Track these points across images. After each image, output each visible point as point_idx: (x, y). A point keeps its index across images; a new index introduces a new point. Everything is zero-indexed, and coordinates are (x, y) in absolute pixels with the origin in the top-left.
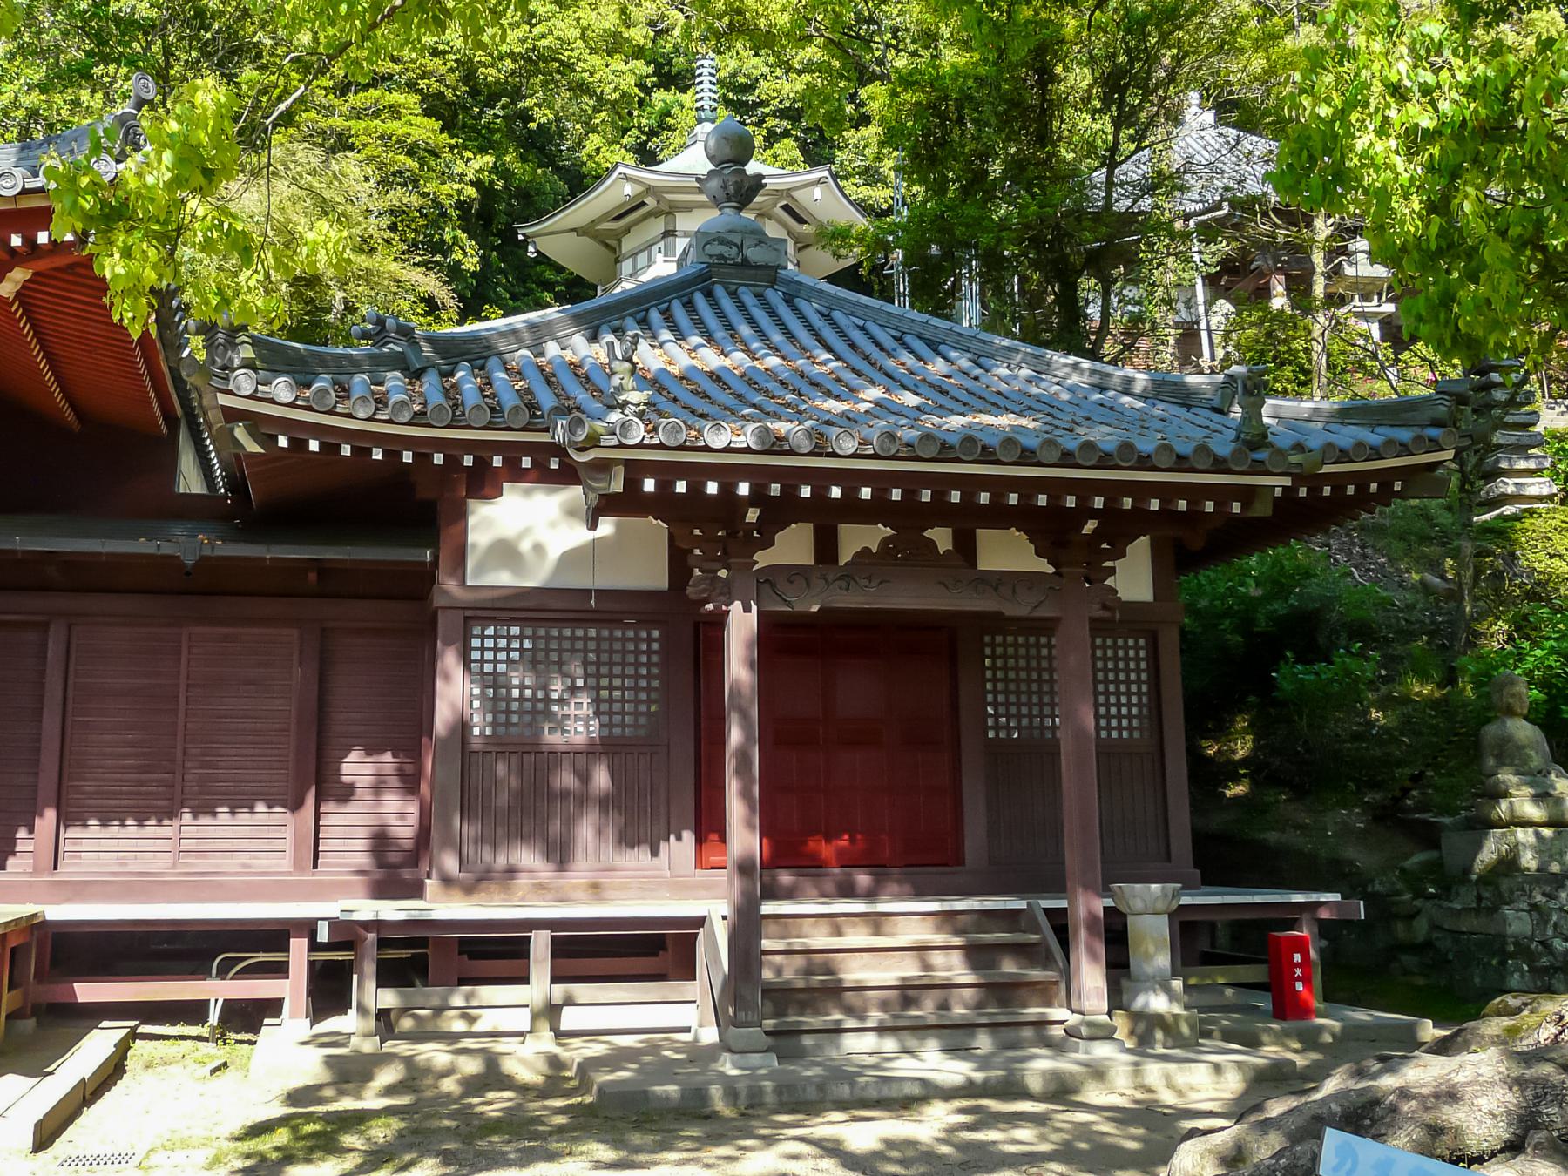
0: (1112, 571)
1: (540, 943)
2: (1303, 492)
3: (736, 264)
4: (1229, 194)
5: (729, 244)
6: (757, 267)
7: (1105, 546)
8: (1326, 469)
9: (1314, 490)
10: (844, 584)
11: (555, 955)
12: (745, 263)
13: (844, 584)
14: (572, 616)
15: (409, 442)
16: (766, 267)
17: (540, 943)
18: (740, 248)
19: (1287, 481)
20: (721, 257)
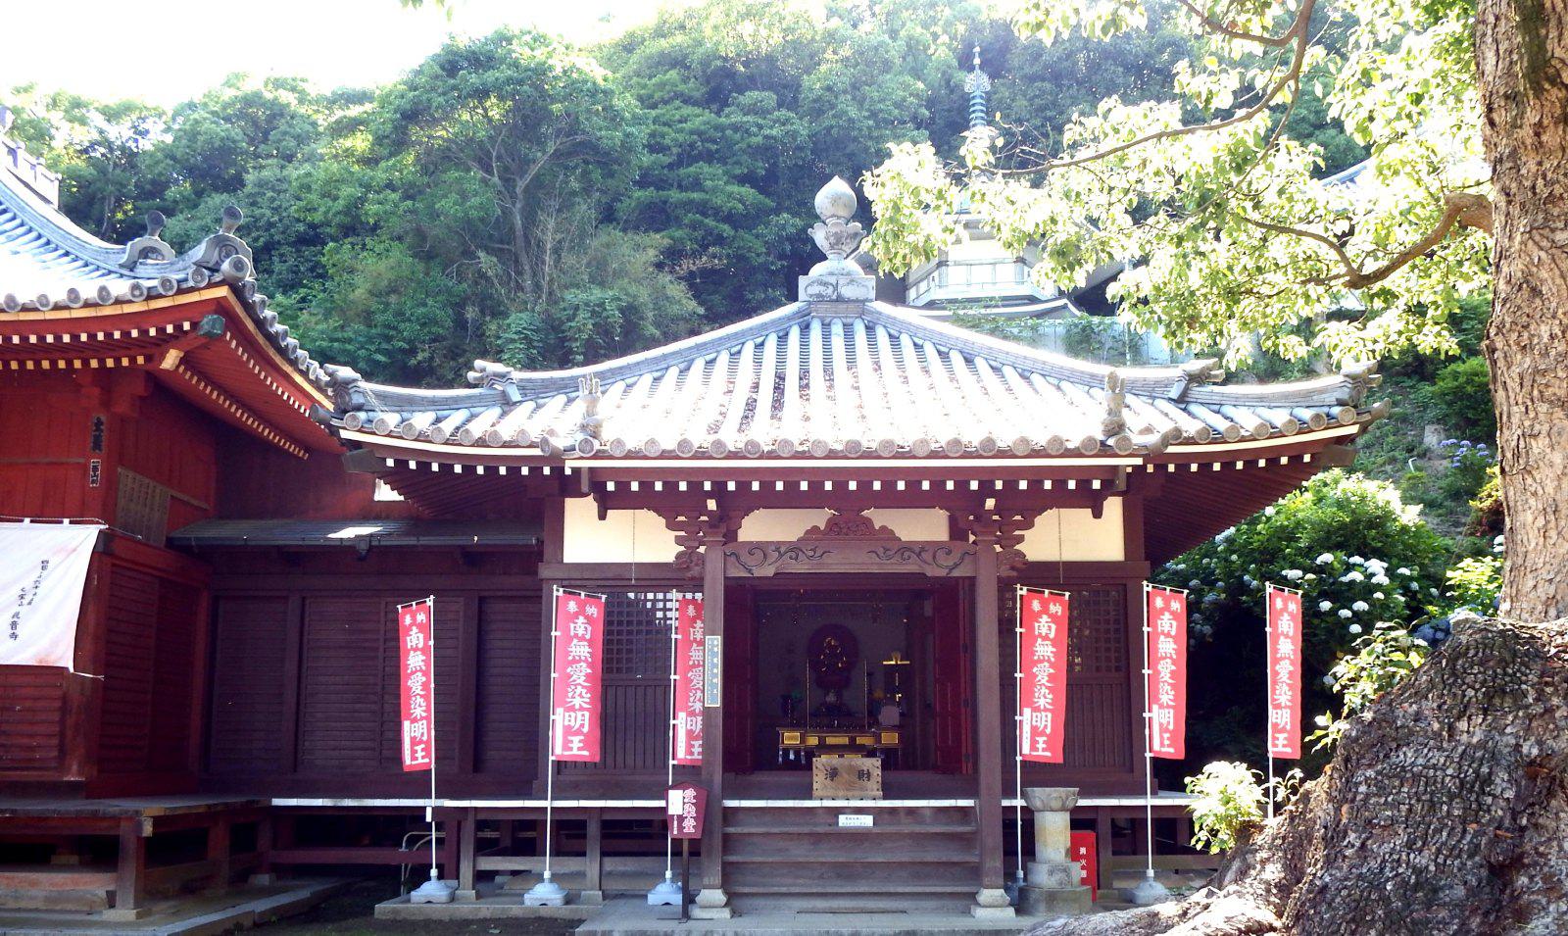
0: (1021, 539)
1: (593, 830)
2: (1150, 469)
3: (832, 301)
4: (1139, 187)
5: (825, 284)
6: (849, 301)
7: (1018, 517)
8: (1171, 449)
9: (1161, 467)
10: (794, 555)
11: (604, 836)
12: (840, 299)
13: (794, 555)
14: (654, 583)
15: (829, 472)
16: (857, 301)
17: (593, 830)
18: (836, 288)
19: (1139, 461)
20: (820, 295)
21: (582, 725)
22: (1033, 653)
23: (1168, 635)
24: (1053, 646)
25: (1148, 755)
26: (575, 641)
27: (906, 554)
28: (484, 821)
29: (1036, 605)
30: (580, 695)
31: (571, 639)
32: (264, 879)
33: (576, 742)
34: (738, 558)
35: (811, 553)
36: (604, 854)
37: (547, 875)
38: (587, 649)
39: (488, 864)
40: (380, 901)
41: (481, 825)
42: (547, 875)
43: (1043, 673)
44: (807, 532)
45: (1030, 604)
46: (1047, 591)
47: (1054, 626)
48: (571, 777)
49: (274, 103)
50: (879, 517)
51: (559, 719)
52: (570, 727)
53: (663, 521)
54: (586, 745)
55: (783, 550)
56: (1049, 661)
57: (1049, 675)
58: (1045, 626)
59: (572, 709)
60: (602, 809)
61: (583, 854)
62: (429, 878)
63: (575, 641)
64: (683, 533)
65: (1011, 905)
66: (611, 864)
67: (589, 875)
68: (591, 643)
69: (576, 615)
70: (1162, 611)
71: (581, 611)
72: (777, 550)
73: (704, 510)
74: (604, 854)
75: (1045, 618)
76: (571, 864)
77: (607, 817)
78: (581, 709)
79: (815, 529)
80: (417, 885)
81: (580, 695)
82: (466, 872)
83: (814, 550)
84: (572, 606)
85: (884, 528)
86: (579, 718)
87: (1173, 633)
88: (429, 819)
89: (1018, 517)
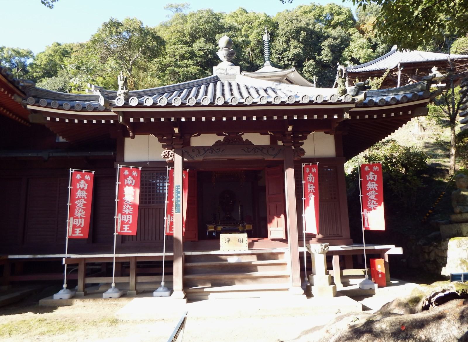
1: (133, 266)
7: (300, 135)
17: (133, 266)
21: (129, 221)
22: (367, 187)
23: (311, 183)
24: (376, 183)
25: (363, 229)
26: (370, 182)
27: (256, 150)
28: (88, 264)
29: (126, 172)
30: (129, 208)
31: (368, 182)
32: (5, 288)
33: (78, 231)
34: (188, 153)
35: (218, 151)
36: (137, 275)
37: (113, 285)
38: (375, 185)
39: (91, 280)
40: (41, 299)
41: (87, 264)
42: (113, 285)
43: (80, 204)
44: (216, 142)
45: (123, 172)
46: (311, 164)
47: (314, 178)
48: (77, 246)
49: (427, 8)
50: (246, 136)
51: (71, 222)
52: (125, 222)
53: (157, 139)
54: (82, 231)
55: (206, 149)
56: (375, 190)
57: (376, 196)
58: (82, 184)
59: (77, 218)
60: (136, 257)
61: (128, 275)
62: (62, 288)
63: (370, 182)
64: (165, 144)
65: (304, 294)
66: (141, 279)
67: (131, 283)
68: (87, 191)
69: (80, 180)
70: (309, 174)
71: (83, 178)
72: (204, 149)
73: (173, 133)
74: (137, 275)
75: (130, 177)
76: (123, 280)
77: (138, 260)
78: (129, 214)
79: (219, 141)
80: (57, 291)
81: (129, 208)
82: (80, 285)
83: (219, 149)
84: (78, 176)
85: (247, 140)
86: (80, 221)
87: (313, 182)
88: (64, 263)
89: (300, 135)
